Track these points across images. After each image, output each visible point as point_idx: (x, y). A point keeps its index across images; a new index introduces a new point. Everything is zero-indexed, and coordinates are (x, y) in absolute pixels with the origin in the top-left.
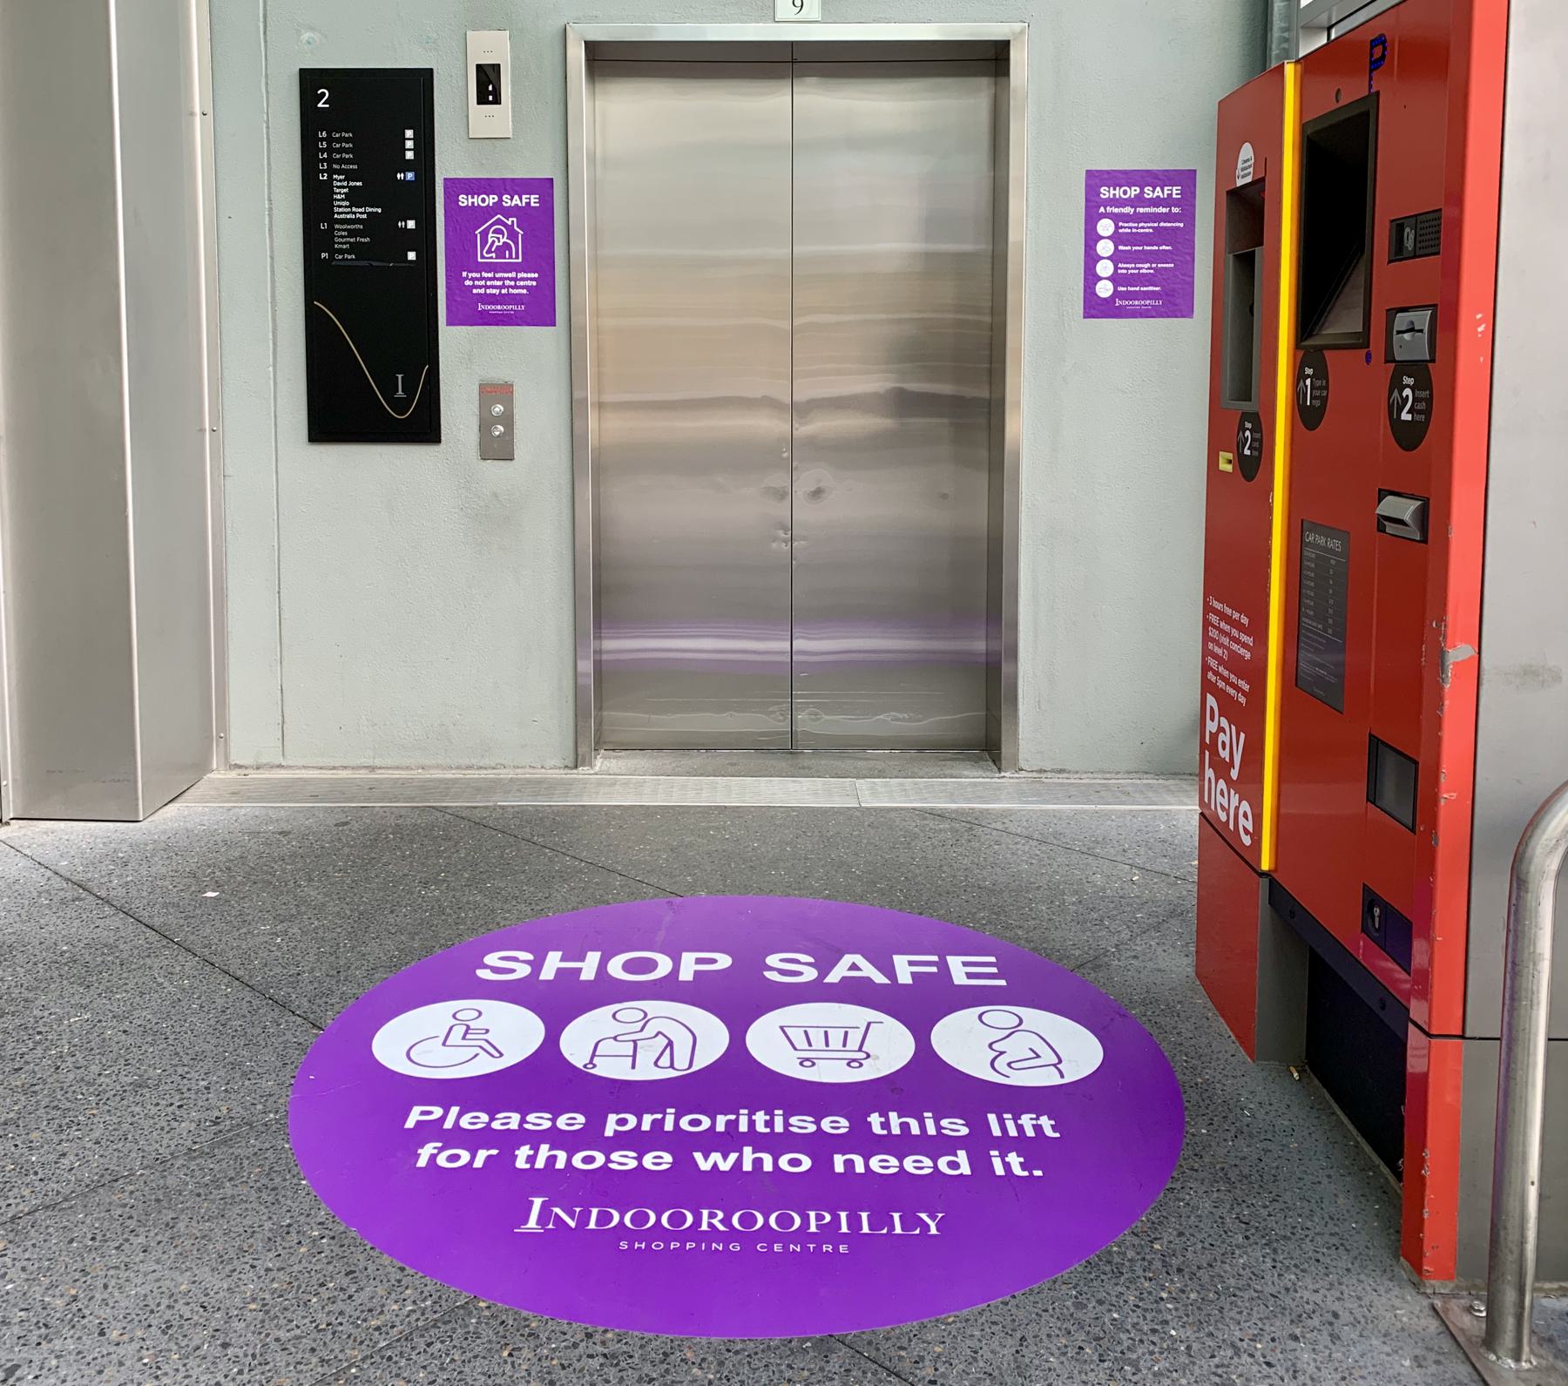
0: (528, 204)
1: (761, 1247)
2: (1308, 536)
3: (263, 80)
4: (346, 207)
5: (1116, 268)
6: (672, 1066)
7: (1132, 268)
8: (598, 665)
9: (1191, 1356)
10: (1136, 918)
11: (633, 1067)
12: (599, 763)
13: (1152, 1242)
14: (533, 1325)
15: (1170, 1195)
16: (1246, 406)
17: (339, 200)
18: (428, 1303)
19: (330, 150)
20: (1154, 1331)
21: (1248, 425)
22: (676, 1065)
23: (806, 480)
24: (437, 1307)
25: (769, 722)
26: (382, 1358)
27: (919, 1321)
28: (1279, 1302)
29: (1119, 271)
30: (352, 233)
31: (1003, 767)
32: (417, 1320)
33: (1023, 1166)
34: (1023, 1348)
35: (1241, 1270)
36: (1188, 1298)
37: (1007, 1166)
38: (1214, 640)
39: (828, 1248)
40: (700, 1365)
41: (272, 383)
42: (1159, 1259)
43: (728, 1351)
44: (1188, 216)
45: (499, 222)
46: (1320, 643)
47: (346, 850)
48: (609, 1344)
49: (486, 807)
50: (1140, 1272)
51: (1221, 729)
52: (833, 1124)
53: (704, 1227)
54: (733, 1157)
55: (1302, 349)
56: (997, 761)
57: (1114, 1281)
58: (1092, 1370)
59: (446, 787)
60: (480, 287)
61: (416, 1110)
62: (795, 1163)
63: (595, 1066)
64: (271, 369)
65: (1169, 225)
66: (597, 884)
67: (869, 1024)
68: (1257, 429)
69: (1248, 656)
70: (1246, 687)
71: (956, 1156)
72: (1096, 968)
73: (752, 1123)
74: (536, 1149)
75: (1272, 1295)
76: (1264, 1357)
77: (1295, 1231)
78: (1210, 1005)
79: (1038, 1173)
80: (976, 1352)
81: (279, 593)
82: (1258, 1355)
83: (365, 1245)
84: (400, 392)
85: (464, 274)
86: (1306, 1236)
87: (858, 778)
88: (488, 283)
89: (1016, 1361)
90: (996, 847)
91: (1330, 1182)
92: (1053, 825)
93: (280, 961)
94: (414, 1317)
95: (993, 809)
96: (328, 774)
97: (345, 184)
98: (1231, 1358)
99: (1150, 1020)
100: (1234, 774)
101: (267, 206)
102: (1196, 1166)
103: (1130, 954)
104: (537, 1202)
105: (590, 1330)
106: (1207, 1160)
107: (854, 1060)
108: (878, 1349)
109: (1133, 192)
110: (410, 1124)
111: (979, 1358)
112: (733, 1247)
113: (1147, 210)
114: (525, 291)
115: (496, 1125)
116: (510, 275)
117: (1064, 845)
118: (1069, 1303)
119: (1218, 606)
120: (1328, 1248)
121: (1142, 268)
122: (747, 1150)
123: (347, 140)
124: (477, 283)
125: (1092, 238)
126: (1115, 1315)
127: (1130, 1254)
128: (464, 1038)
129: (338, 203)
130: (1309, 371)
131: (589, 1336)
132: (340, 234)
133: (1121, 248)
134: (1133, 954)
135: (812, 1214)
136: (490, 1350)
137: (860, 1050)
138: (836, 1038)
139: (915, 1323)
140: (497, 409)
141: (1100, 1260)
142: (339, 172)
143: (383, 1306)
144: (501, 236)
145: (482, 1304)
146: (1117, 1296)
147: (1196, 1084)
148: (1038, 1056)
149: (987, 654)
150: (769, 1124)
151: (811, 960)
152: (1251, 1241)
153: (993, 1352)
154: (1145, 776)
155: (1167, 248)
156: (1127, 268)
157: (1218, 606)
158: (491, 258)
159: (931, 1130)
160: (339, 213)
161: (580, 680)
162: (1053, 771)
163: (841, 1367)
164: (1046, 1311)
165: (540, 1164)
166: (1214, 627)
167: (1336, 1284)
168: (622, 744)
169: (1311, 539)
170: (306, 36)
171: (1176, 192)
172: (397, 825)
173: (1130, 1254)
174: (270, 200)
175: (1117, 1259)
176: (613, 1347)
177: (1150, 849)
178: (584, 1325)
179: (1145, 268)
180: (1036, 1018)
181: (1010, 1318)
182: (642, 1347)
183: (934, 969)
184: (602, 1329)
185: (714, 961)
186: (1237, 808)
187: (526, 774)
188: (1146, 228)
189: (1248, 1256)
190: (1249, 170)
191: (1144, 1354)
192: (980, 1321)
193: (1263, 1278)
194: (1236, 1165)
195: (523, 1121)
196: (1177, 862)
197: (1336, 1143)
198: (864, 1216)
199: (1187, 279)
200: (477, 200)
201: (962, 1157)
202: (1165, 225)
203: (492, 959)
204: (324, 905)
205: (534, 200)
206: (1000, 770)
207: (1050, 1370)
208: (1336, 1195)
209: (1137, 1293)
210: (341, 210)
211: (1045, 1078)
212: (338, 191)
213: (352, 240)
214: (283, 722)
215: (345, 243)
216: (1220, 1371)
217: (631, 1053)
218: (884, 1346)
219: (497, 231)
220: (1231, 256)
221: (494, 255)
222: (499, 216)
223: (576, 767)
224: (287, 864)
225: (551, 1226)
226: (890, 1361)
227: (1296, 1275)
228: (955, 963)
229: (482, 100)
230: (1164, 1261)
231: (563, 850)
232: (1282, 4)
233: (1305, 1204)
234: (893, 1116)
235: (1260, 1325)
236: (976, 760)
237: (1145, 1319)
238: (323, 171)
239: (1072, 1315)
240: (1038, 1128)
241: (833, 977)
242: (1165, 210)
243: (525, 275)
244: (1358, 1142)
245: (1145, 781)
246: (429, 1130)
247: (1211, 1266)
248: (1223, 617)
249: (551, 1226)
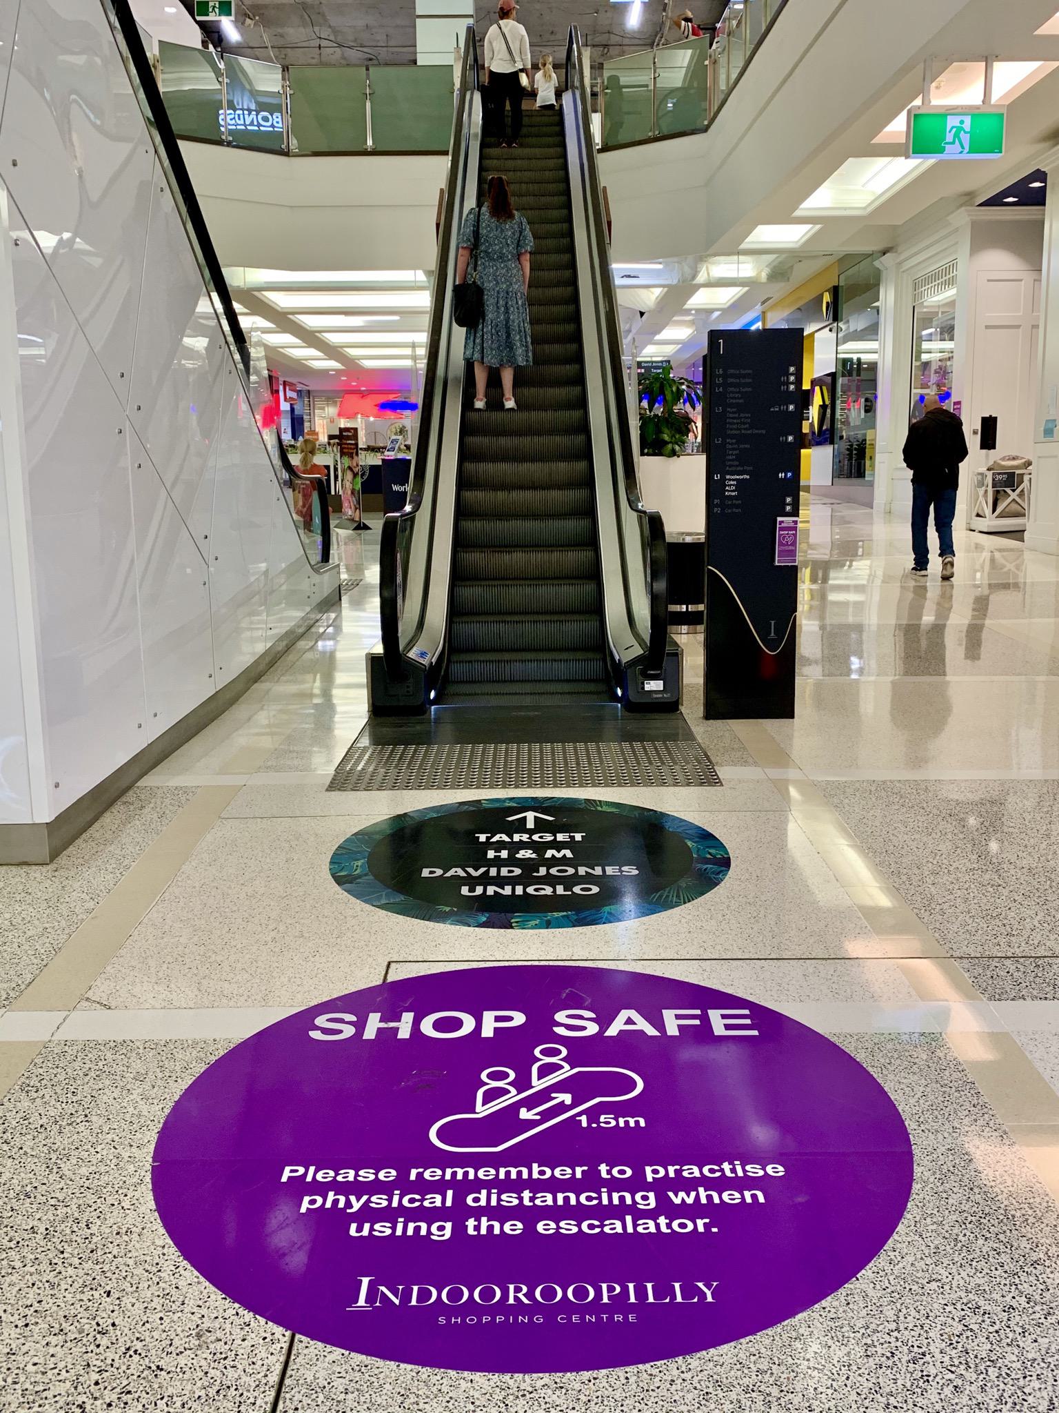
17: (730, 460)
39: (618, 1318)
97: (736, 446)
104: (365, 1281)
112: (537, 1319)
135: (604, 1286)
183: (697, 1022)
185: (510, 1019)
198: (649, 1286)
212: (730, 452)
241: (612, 1031)
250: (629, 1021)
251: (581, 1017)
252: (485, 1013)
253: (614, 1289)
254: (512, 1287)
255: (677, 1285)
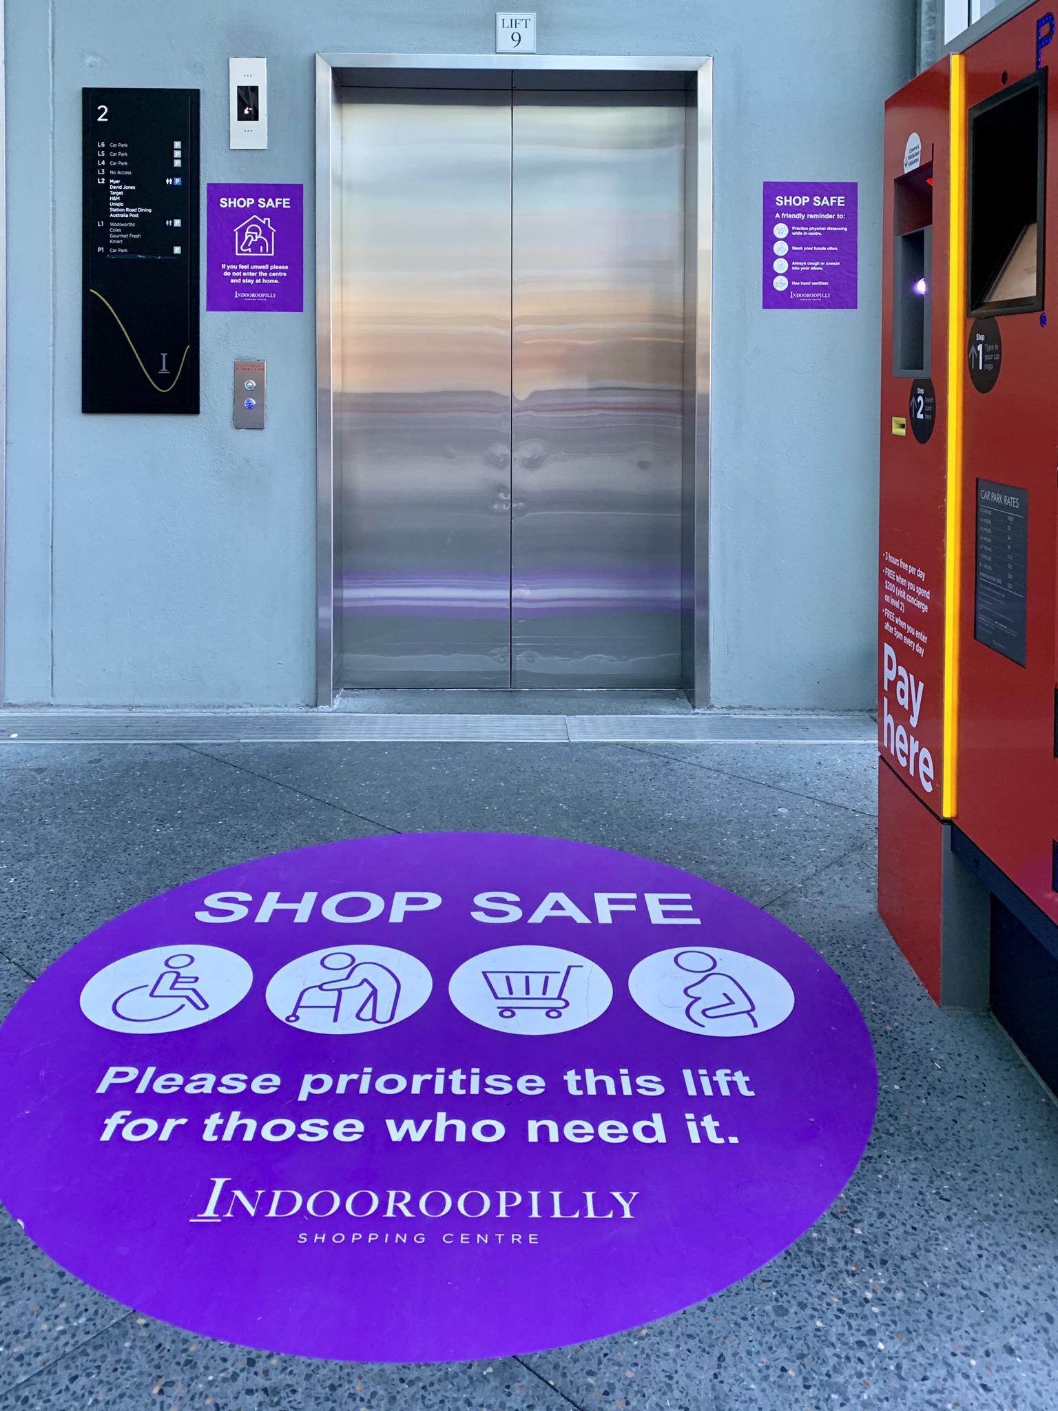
0: (281, 206)
1: (448, 1238)
2: (983, 493)
3: (51, 97)
4: (121, 207)
5: (790, 266)
6: (374, 1019)
7: (804, 266)
8: (339, 612)
9: (901, 1378)
10: (820, 852)
11: (335, 1020)
12: (337, 702)
13: (852, 1225)
14: (192, 1349)
15: (868, 1166)
16: (918, 374)
17: (114, 202)
18: (82, 1320)
19: (108, 158)
20: (860, 1344)
21: (921, 391)
22: (378, 1018)
23: (525, 451)
24: (91, 1328)
25: (492, 662)
26: (17, 1398)
27: (610, 1336)
28: (989, 1303)
29: (793, 268)
30: (125, 230)
31: (696, 706)
32: (66, 1344)
33: (720, 1132)
34: (722, 1370)
35: (946, 1261)
36: (894, 1299)
37: (702, 1131)
38: (889, 593)
39: (516, 1238)
40: (369, 1402)
41: (51, 360)
42: (860, 1247)
43: (402, 1381)
44: (851, 221)
45: (255, 221)
46: (1000, 598)
47: (94, 787)
48: (272, 1373)
49: (229, 745)
50: (841, 1265)
51: (899, 678)
52: (532, 1084)
53: (390, 1213)
54: (426, 1124)
55: (972, 317)
56: (691, 697)
57: (815, 1277)
58: (797, 1400)
59: (196, 727)
60: (237, 278)
61: (112, 1070)
62: (489, 1131)
63: (297, 1018)
64: (51, 348)
65: (835, 229)
66: (322, 821)
67: (569, 968)
68: (929, 393)
69: (925, 609)
70: (924, 639)
71: (652, 1121)
72: (784, 905)
73: (448, 1084)
74: (226, 1117)
75: (981, 1293)
76: (980, 1378)
77: (997, 1209)
78: (893, 943)
79: (734, 1140)
80: (671, 1378)
81: (52, 547)
82: (973, 1374)
83: (28, 1243)
84: (164, 369)
85: (223, 266)
86: (1010, 1215)
87: (568, 715)
88: (244, 274)
89: (714, 1389)
90: (690, 781)
91: (1027, 1148)
92: (741, 760)
93: (9, 903)
94: (63, 1339)
95: (688, 744)
96: (91, 713)
97: (120, 187)
98: (945, 1380)
99: (837, 961)
100: (914, 721)
101: (51, 206)
102: (892, 1130)
103: (815, 889)
104: (219, 1183)
105: (253, 1355)
106: (902, 1121)
107: (553, 1009)
108: (564, 1375)
109: (804, 200)
110: (102, 1089)
111: (674, 1386)
112: (418, 1239)
113: (816, 216)
114: (276, 281)
115: (190, 1089)
116: (263, 267)
117: (752, 779)
118: (768, 1308)
119: (894, 561)
120: (1033, 1230)
121: (812, 266)
122: (441, 1116)
123: (123, 150)
124: (234, 274)
125: (769, 240)
126: (819, 1324)
127: (831, 1241)
128: (172, 988)
129: (113, 204)
130: (980, 337)
131: (251, 1362)
132: (114, 230)
133: (794, 248)
134: (819, 889)
135: (503, 1195)
136: (138, 1386)
137: (559, 998)
138: (536, 983)
139: (605, 1338)
140: (250, 384)
141: (800, 1250)
142: (115, 178)
143: (31, 1325)
144: (256, 233)
145: (141, 1321)
146: (819, 1298)
147: (886, 1032)
148: (732, 1002)
149: (682, 601)
150: (465, 1084)
151: (517, 899)
152: (954, 1222)
153: (688, 1376)
154: (822, 712)
155: (833, 249)
156: (799, 266)
157: (894, 561)
158: (248, 252)
159: (627, 1091)
160: (114, 213)
161: (321, 625)
162: (741, 707)
163: (523, 1401)
164: (745, 1319)
165: (228, 1136)
166: (890, 580)
167: (1046, 1277)
168: (360, 684)
169: (987, 496)
170: (89, 59)
171: (840, 201)
172: (146, 762)
173: (831, 1241)
174: (53, 201)
175: (817, 1248)
176: (277, 1378)
177: (829, 782)
178: (247, 1349)
179: (815, 266)
180: (730, 960)
181: (706, 1329)
182: (308, 1377)
183: (632, 908)
184: (267, 1353)
185: (424, 901)
186: (917, 755)
187: (270, 711)
188: (816, 231)
189: (953, 1242)
190: (916, 158)
191: (851, 1377)
192: (676, 1334)
193: (970, 1271)
194: (931, 1128)
195: (218, 1083)
196: (854, 795)
197: (1028, 1100)
198: (556, 1195)
199: (851, 275)
200: (236, 203)
201: (657, 1121)
202: (831, 229)
203: (212, 901)
204: (62, 842)
205: (286, 203)
206: (694, 707)
207: (751, 1400)
208: (1034, 1164)
209: (840, 1293)
210: (116, 210)
211: (739, 1027)
212: (114, 193)
213: (125, 236)
214: (53, 665)
215: (119, 239)
216: (934, 1398)
217: (335, 1004)
218: (574, 1369)
219: (253, 229)
220: (899, 238)
221: (250, 250)
222: (255, 216)
223: (316, 706)
224: (36, 801)
225: (229, 1215)
226: (578, 1392)
227: (1004, 1266)
228: (652, 899)
229: (242, 117)
230: (867, 1250)
231: (295, 787)
232: (928, 42)
233: (1006, 1175)
234: (589, 1073)
235: (972, 1335)
236: (674, 696)
237: (850, 1327)
238: (101, 177)
239: (772, 1324)
240: (732, 1085)
241: (537, 917)
242: (831, 216)
243: (277, 267)
244: (1050, 1099)
245: (822, 717)
246: (123, 1096)
247: (915, 1256)
248: (898, 570)
249: (229, 1215)
250: (557, 906)
251: (503, 901)
252: (397, 895)
253: (514, 1199)
254: (392, 1194)
255: (589, 1195)
